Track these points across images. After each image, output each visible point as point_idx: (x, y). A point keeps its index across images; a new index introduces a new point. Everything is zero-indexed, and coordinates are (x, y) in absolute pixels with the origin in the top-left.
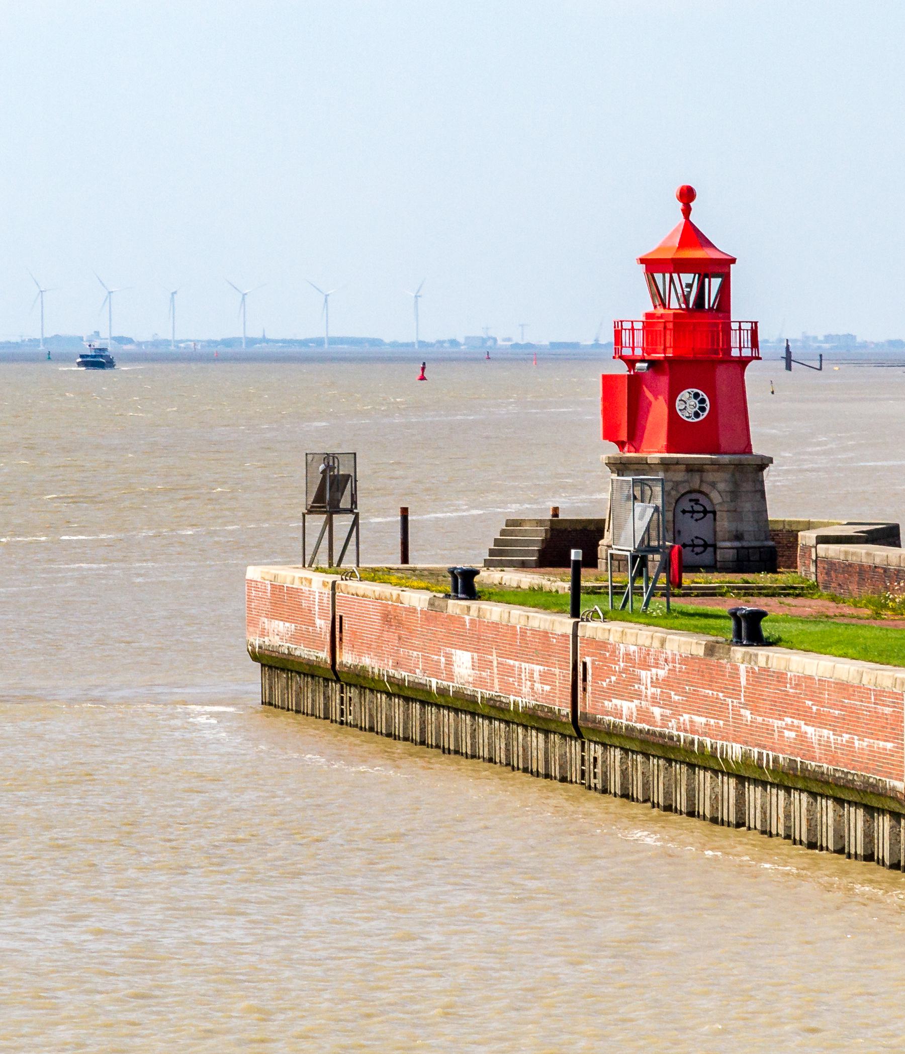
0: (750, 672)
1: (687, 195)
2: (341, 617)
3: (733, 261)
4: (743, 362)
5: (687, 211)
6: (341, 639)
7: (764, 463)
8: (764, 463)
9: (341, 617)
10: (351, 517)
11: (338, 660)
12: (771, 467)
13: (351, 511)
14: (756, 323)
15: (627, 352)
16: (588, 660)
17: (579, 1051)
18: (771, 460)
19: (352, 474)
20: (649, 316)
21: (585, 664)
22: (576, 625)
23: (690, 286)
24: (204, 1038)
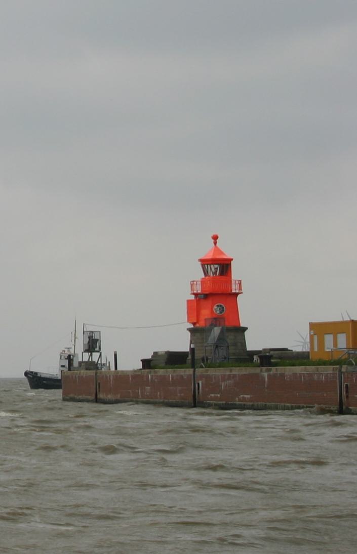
0: (269, 376)
1: (215, 238)
2: (99, 384)
3: (232, 259)
4: (236, 295)
5: (215, 243)
6: (99, 391)
7: (245, 329)
8: (245, 329)
9: (99, 384)
10: (99, 354)
11: (98, 396)
12: (247, 331)
13: (98, 352)
14: (241, 281)
15: (195, 292)
16: (200, 382)
17: (60, 551)
18: (247, 328)
19: (99, 338)
20: (203, 279)
21: (198, 384)
22: (194, 371)
23: (217, 269)
24: (14, 514)
